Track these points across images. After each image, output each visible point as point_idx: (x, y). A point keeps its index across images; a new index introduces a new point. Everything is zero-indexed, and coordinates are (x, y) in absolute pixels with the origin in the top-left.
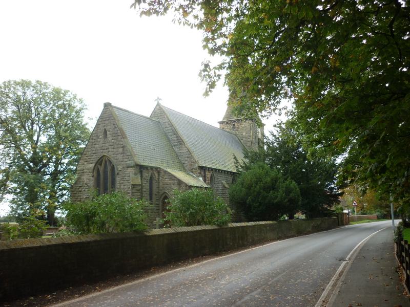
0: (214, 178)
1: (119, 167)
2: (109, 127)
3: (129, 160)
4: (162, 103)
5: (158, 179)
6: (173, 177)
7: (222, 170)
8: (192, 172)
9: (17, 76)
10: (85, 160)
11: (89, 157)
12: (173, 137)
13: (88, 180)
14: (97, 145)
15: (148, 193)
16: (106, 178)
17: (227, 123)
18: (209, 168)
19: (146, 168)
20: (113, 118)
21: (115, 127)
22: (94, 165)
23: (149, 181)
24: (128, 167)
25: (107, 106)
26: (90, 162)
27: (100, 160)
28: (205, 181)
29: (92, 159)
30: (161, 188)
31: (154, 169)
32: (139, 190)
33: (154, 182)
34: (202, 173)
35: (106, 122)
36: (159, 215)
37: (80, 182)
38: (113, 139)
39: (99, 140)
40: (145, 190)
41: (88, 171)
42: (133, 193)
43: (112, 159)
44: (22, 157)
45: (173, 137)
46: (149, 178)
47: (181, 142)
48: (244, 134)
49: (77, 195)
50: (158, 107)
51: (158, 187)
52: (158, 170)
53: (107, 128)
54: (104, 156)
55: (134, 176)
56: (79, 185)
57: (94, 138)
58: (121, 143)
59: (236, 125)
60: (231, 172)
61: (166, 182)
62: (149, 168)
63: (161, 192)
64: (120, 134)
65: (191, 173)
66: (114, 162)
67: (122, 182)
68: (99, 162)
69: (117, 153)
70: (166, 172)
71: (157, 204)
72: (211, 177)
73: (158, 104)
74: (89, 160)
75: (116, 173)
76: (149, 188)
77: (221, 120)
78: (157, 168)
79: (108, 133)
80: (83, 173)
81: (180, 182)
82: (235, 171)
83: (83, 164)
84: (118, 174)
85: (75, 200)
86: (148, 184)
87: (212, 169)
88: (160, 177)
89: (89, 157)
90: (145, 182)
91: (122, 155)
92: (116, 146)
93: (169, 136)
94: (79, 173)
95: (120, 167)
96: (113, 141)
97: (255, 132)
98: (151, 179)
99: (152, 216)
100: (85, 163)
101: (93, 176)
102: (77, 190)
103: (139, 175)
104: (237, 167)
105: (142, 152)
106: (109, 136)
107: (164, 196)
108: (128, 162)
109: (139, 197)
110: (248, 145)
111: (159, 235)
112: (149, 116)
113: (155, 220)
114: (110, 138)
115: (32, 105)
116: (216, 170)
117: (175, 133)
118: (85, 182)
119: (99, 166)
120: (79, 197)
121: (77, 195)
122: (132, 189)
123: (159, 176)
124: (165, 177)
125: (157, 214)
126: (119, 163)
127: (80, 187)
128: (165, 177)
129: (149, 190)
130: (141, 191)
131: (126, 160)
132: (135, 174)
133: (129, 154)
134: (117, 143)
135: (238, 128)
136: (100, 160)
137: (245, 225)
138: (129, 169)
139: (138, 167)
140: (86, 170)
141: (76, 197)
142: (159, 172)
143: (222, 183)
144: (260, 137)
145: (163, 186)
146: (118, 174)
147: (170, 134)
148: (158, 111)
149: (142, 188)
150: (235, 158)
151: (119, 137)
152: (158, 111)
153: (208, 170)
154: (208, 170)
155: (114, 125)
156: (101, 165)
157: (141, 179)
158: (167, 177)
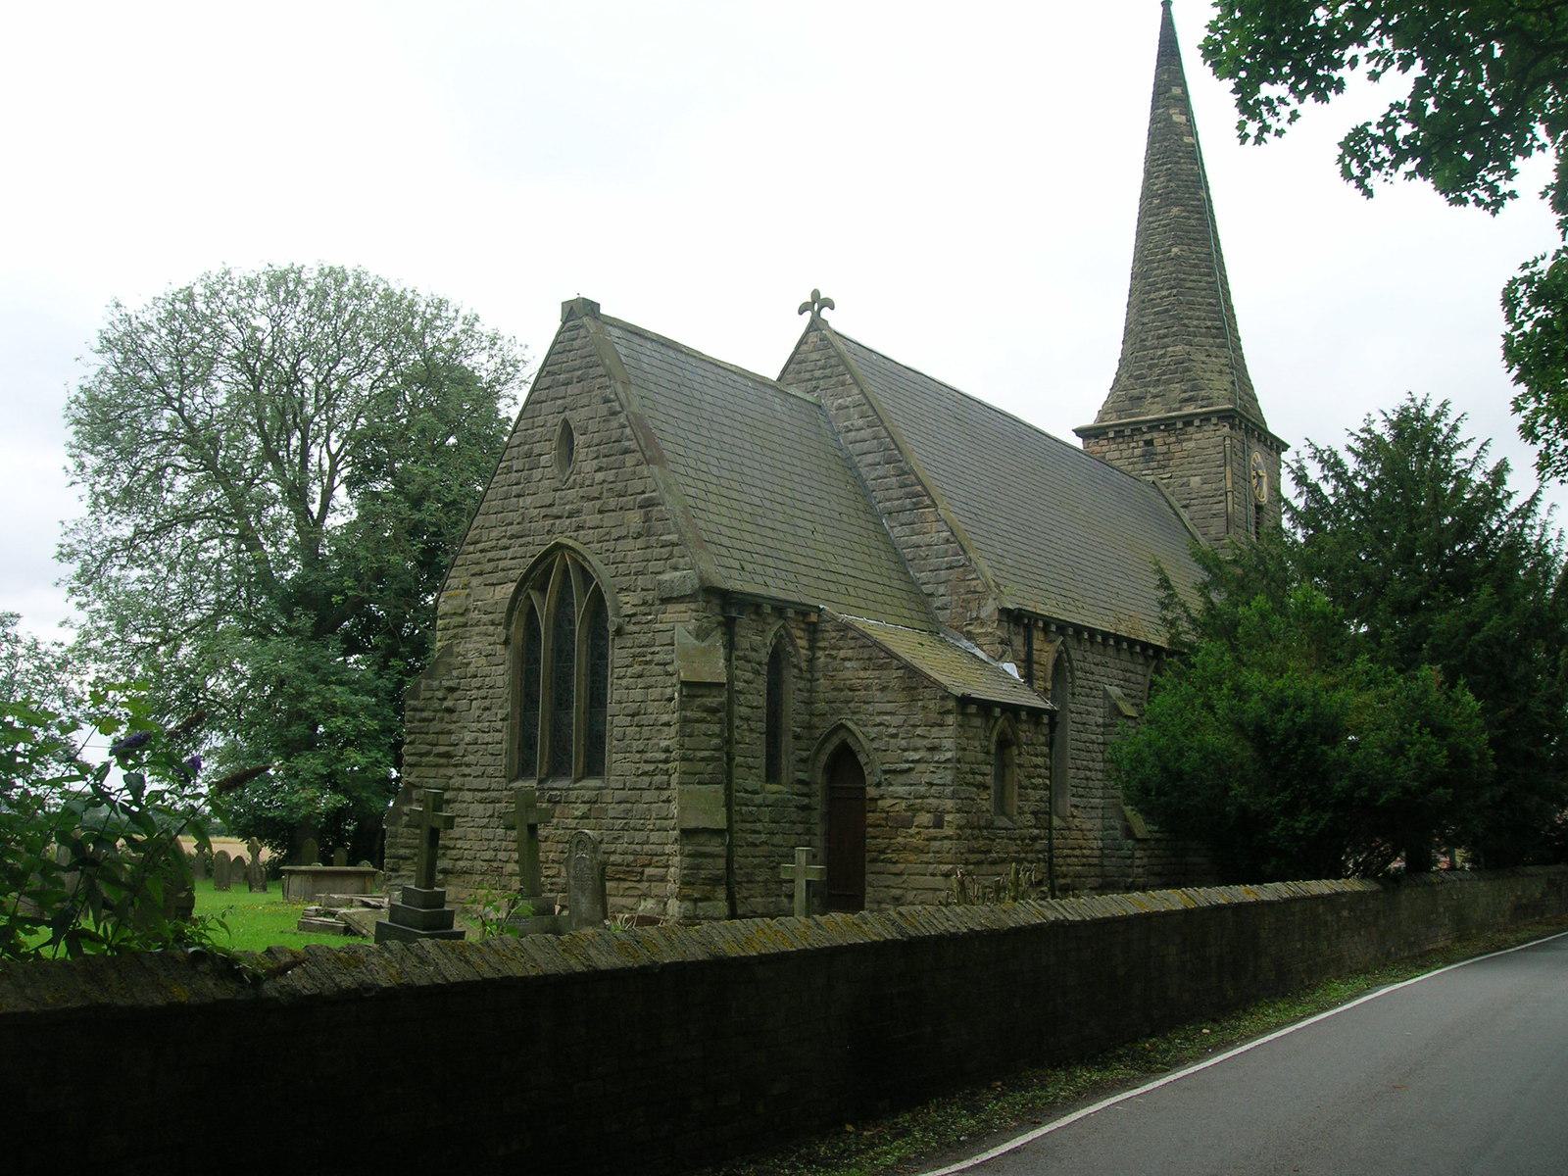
0: (1072, 672)
1: (623, 598)
2: (584, 413)
3: (676, 569)
4: (835, 320)
5: (811, 660)
6: (880, 657)
7: (1106, 635)
8: (970, 636)
9: (250, 262)
10: (477, 569)
11: (490, 555)
12: (880, 471)
13: (483, 661)
14: (529, 499)
15: (762, 726)
16: (562, 652)
17: (1119, 434)
18: (1048, 621)
19: (752, 604)
20: (601, 370)
21: (615, 414)
22: (511, 587)
23: (764, 670)
24: (665, 601)
25: (580, 314)
26: (494, 578)
27: (542, 567)
28: (1029, 677)
29: (501, 564)
30: (821, 706)
31: (790, 613)
32: (713, 711)
33: (790, 675)
34: (1018, 642)
35: (570, 390)
36: (808, 832)
37: (450, 668)
38: (600, 469)
39: (537, 474)
40: (744, 711)
41: (486, 618)
42: (685, 721)
43: (595, 560)
44: (265, 581)
45: (880, 471)
46: (764, 656)
47: (919, 497)
48: (1195, 481)
49: (436, 726)
50: (813, 338)
51: (809, 703)
52: (809, 619)
53: (576, 418)
54: (559, 546)
55: (692, 640)
56: (446, 683)
57: (516, 465)
58: (638, 485)
59: (1158, 442)
60: (1146, 646)
61: (848, 674)
62: (768, 609)
63: (823, 727)
64: (632, 445)
65: (965, 643)
66: (603, 573)
67: (637, 669)
68: (537, 575)
69: (615, 534)
70: (846, 628)
71: (800, 782)
72: (1058, 664)
73: (816, 325)
74: (489, 567)
75: (612, 629)
76: (762, 701)
77: (1089, 419)
78: (803, 611)
79: (579, 440)
80: (465, 625)
81: (914, 680)
82: (1161, 641)
83: (466, 586)
84: (619, 632)
85: (425, 748)
86: (761, 684)
87: (1062, 627)
88: (820, 653)
89: (490, 555)
90: (749, 676)
91: (640, 543)
92: (612, 503)
93: (863, 471)
94: (445, 629)
95: (629, 602)
96: (600, 476)
97: (1244, 476)
98: (777, 660)
99: (777, 839)
100: (475, 582)
101: (506, 642)
102: (436, 704)
103: (717, 640)
104: (1172, 624)
105: (735, 533)
106: (580, 453)
107: (835, 741)
108: (666, 577)
109: (715, 741)
110: (1213, 531)
111: (803, 954)
112: (772, 373)
113: (791, 858)
114: (585, 462)
115: (306, 364)
116: (1079, 630)
117: (894, 455)
118: (471, 669)
119: (535, 596)
120: (443, 738)
121: (436, 726)
122: (683, 706)
123: (812, 648)
124: (842, 654)
125: (800, 828)
126: (625, 582)
127: (451, 690)
128: (842, 654)
129: (763, 713)
130: (725, 714)
131: (653, 566)
132: (701, 634)
133: (674, 537)
134: (620, 486)
135: (1168, 456)
136: (542, 567)
137: (1251, 898)
138: (670, 607)
139: (716, 601)
140: (475, 615)
141: (431, 738)
142: (813, 631)
143: (1106, 695)
144: (1264, 500)
145: (830, 695)
146: (619, 632)
147: (869, 459)
148: (815, 356)
149: (730, 701)
150: (1165, 584)
151: (630, 460)
152: (815, 356)
153: (1047, 625)
154: (1046, 630)
155: (607, 401)
156: (543, 589)
157: (728, 660)
158: (850, 653)
